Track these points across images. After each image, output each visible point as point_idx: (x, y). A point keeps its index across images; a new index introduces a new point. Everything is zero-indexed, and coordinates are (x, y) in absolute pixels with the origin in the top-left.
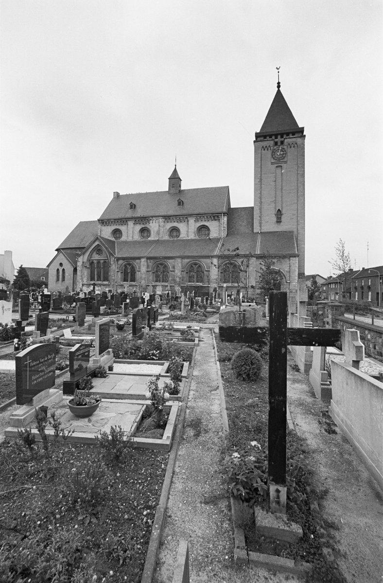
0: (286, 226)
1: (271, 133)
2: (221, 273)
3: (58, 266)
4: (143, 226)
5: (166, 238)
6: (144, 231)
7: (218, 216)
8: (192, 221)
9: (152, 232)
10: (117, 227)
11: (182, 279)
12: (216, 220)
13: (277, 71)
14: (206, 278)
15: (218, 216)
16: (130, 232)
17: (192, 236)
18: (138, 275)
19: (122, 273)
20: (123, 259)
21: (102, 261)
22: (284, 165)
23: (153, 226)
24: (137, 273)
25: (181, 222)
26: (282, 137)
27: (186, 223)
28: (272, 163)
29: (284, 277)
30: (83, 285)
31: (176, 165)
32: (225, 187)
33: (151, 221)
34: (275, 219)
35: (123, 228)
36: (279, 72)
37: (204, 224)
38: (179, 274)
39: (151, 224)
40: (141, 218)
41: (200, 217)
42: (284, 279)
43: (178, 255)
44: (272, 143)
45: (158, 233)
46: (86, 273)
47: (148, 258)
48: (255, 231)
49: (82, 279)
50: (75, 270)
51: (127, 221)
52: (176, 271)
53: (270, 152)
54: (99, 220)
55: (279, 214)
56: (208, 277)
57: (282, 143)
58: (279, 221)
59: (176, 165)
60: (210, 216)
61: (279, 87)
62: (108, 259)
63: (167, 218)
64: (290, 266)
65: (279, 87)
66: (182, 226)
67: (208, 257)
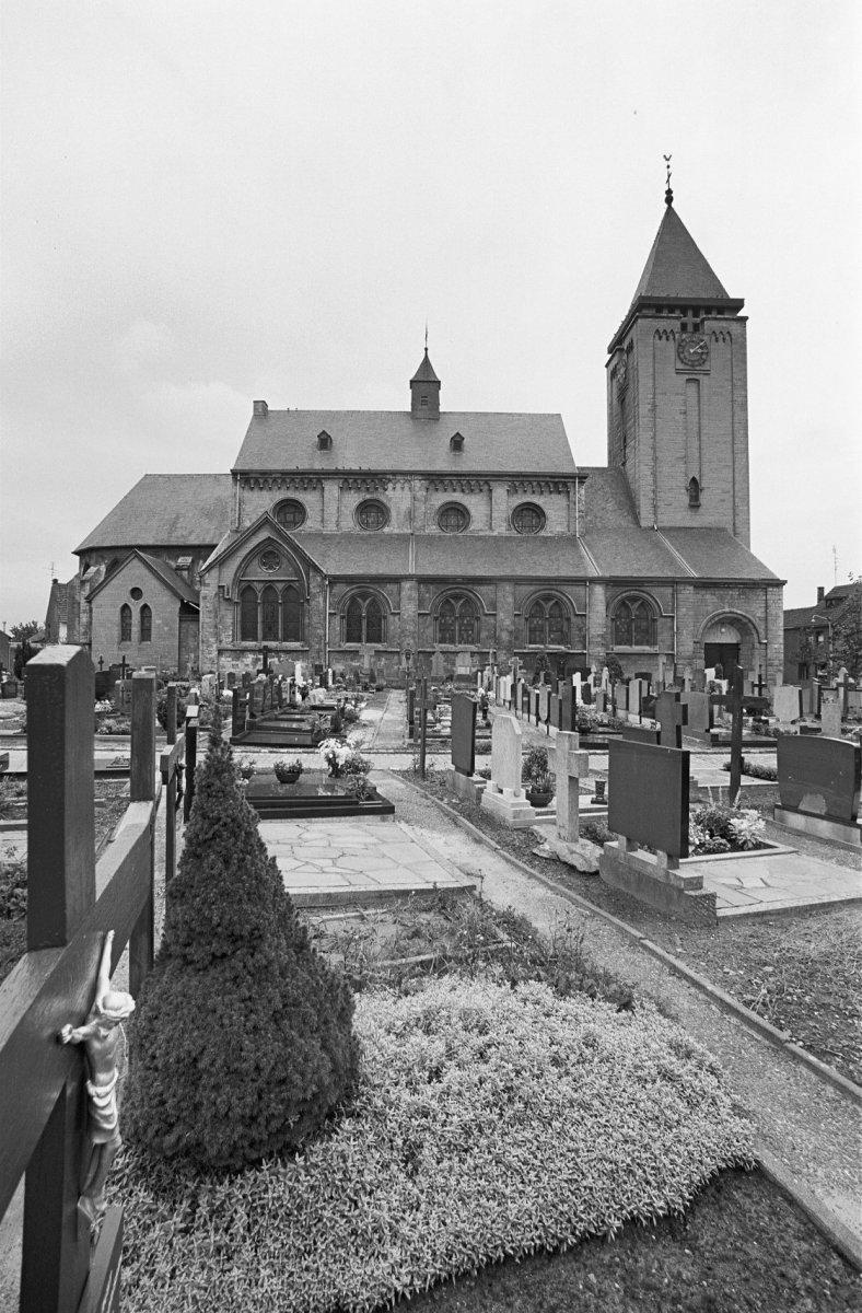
0: (713, 513)
1: (688, 303)
2: (613, 620)
3: (127, 598)
4: (368, 496)
5: (433, 529)
6: (372, 511)
7: (565, 484)
8: (500, 492)
9: (393, 513)
10: (291, 494)
11: (515, 634)
12: (559, 493)
13: (666, 163)
14: (575, 632)
15: (565, 484)
16: (331, 509)
17: (501, 529)
18: (393, 625)
19: (342, 618)
20: (349, 580)
21: (280, 586)
22: (704, 379)
23: (398, 498)
24: (391, 618)
25: (472, 491)
26: (696, 315)
27: (486, 493)
28: (678, 372)
29: (754, 632)
30: (221, 652)
31: (426, 349)
32: (553, 415)
33: (390, 486)
34: (686, 499)
35: (308, 499)
36: (668, 167)
37: (454, 499)
38: (508, 622)
39: (389, 493)
40: (360, 474)
41: (522, 483)
42: (755, 636)
43: (507, 572)
44: (676, 325)
45: (411, 516)
46: (229, 617)
47: (423, 580)
48: (644, 524)
49: (217, 635)
50: (189, 612)
51: (319, 480)
52: (501, 615)
53: (671, 347)
54: (234, 473)
55: (695, 487)
56: (580, 630)
57: (697, 327)
58: (695, 504)
59: (426, 349)
60: (547, 483)
61: (669, 200)
62: (300, 580)
63: (435, 479)
64: (766, 607)
65: (669, 200)
66: (474, 503)
67: (585, 581)
